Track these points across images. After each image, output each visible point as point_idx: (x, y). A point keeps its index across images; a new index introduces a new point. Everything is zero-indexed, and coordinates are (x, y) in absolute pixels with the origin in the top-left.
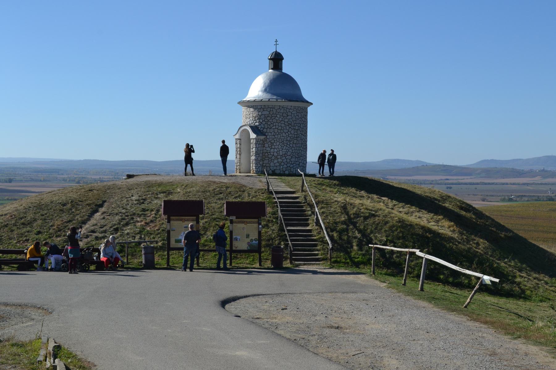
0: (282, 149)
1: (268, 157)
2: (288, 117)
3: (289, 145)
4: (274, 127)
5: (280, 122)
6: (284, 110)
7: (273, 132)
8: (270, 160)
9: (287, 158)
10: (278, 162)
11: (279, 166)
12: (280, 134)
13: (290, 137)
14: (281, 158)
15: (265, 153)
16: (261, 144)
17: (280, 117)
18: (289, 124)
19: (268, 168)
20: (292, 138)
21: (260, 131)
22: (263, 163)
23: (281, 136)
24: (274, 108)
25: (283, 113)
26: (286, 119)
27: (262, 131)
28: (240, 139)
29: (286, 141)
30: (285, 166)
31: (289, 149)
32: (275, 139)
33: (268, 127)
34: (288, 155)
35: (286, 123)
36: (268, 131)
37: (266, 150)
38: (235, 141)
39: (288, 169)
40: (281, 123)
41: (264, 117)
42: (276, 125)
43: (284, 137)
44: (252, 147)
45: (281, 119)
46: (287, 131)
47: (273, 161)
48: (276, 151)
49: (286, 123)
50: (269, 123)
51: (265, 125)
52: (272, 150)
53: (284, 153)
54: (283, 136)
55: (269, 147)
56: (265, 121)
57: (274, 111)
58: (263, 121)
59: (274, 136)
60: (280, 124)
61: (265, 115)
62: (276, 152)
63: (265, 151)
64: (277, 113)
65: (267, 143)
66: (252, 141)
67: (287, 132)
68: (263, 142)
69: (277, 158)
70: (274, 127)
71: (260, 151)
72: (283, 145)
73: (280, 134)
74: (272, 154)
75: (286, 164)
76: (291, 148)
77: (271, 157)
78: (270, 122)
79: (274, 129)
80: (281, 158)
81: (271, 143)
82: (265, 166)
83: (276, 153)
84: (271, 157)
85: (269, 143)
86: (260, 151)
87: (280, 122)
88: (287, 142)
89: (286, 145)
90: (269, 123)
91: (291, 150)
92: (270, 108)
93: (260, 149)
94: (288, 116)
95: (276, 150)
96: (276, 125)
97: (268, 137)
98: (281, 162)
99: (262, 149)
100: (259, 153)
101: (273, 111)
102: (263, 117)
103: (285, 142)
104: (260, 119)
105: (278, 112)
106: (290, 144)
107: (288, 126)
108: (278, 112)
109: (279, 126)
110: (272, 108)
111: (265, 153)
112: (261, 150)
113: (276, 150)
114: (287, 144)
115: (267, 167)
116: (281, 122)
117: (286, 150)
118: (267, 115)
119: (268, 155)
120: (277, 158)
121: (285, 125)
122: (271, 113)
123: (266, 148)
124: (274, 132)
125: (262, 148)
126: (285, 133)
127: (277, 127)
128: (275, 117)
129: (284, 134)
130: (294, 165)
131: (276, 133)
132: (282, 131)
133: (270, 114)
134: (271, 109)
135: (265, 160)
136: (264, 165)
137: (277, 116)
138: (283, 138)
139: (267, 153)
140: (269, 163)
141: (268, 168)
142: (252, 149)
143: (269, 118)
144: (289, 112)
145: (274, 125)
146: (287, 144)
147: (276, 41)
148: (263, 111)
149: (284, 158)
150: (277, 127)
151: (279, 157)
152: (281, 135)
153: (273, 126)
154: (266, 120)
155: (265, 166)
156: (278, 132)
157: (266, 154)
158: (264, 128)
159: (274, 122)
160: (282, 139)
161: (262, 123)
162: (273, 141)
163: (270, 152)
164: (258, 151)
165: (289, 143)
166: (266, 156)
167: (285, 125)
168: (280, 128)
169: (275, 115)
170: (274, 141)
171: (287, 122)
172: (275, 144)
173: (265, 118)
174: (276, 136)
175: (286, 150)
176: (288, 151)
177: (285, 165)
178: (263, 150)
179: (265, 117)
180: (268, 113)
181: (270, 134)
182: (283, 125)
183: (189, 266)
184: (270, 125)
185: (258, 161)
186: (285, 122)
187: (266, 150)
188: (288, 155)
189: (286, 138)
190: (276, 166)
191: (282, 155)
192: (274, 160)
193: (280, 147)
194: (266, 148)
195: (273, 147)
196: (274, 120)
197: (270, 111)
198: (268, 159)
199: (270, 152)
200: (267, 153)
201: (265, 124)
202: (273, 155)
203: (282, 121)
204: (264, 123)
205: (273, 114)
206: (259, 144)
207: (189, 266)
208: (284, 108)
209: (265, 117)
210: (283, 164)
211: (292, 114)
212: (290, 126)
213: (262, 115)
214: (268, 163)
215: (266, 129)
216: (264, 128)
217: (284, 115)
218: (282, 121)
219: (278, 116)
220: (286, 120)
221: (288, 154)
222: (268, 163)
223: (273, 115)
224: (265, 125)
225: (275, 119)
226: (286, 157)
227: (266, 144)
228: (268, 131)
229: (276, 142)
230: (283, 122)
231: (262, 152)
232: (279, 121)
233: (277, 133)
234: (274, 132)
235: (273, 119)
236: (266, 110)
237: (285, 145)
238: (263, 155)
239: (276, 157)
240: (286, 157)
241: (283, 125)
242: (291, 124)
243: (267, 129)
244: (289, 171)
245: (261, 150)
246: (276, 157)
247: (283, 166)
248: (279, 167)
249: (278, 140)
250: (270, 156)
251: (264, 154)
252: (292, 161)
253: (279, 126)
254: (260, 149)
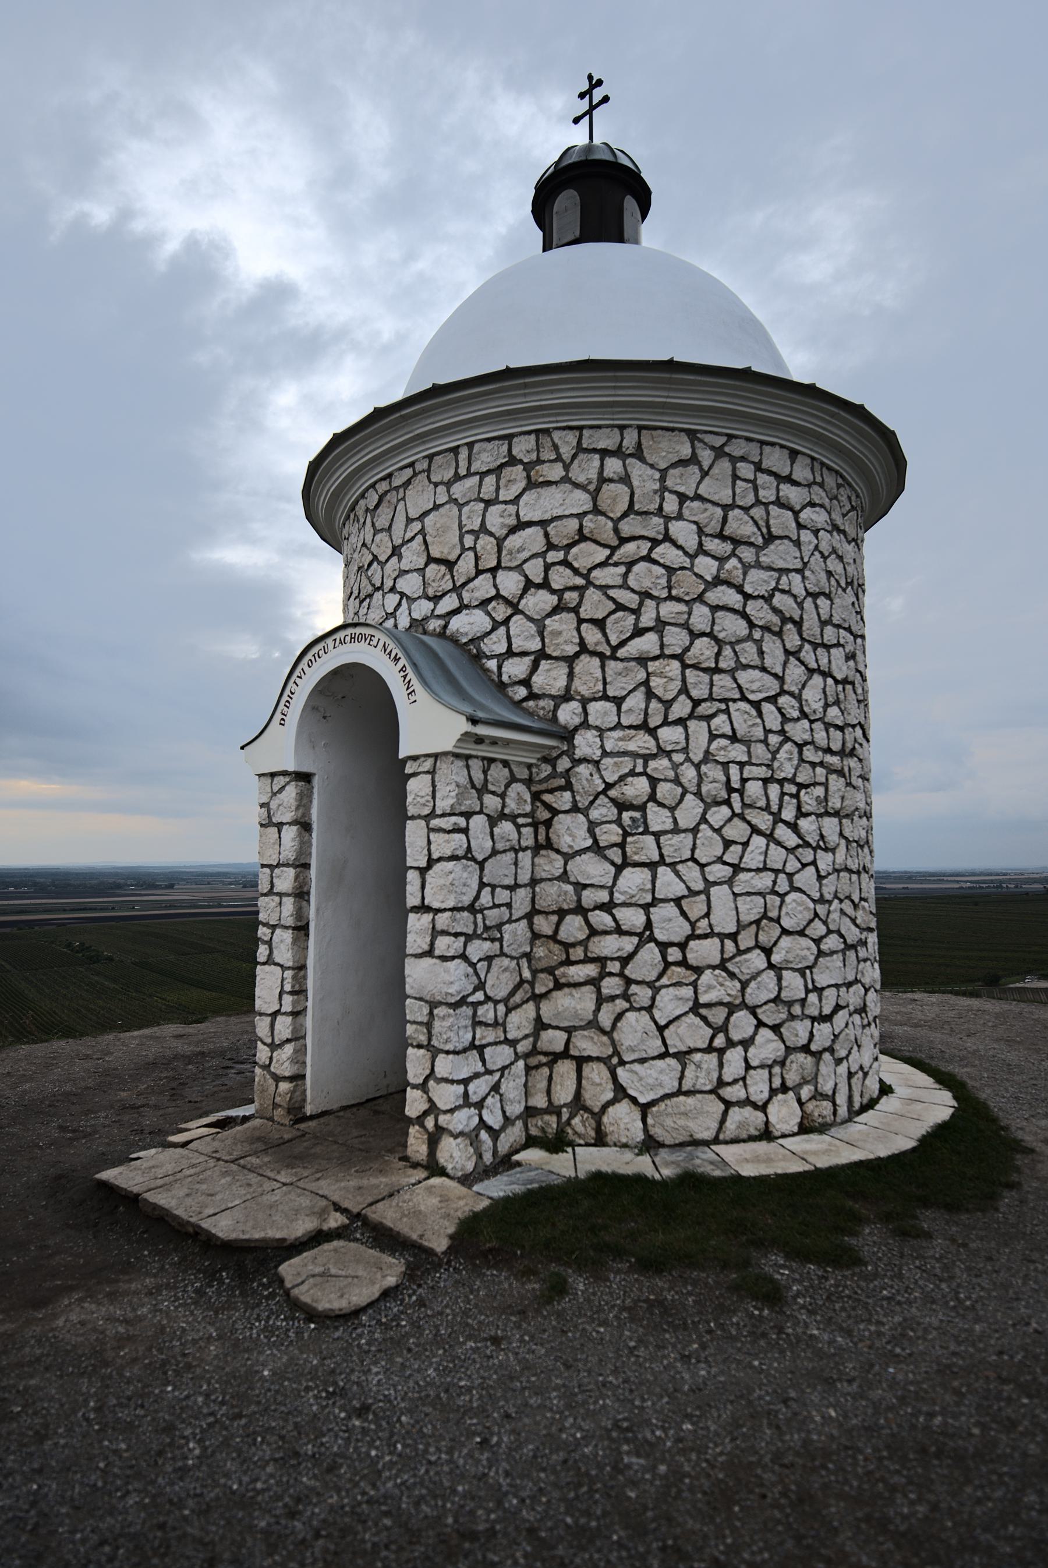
0: (737, 868)
1: (587, 960)
2: (779, 554)
3: (794, 827)
4: (648, 643)
5: (700, 598)
6: (735, 477)
7: (639, 696)
8: (611, 986)
9: (776, 958)
10: (696, 1008)
11: (709, 1049)
12: (704, 709)
13: (800, 747)
14: (722, 966)
15: (562, 913)
16: (513, 818)
17: (701, 550)
18: (785, 620)
19: (596, 1073)
20: (809, 754)
21: (502, 686)
22: (540, 1025)
23: (713, 737)
24: (639, 454)
25: (726, 508)
26: (758, 565)
27: (526, 683)
28: (304, 777)
29: (766, 781)
30: (767, 1048)
31: (792, 865)
32: (660, 766)
33: (583, 648)
34: (785, 932)
35: (758, 611)
36: (581, 687)
37: (564, 877)
38: (255, 792)
39: (792, 1078)
40: (715, 608)
41: (539, 545)
42: (660, 626)
43: (747, 743)
44: (415, 857)
45: (707, 566)
46: (774, 687)
47: (642, 995)
48: (680, 890)
49: (758, 611)
50: (594, 605)
51: (552, 624)
52: (633, 880)
53: (751, 909)
54: (734, 738)
55: (597, 848)
56: (545, 585)
57: (644, 478)
58: (529, 585)
59: (652, 732)
60: (700, 617)
61: (543, 523)
62: (678, 901)
63: (552, 894)
64: (671, 505)
65: (575, 809)
66: (417, 788)
67: (772, 699)
68: (536, 796)
69: (684, 963)
70: (648, 643)
71: (503, 896)
72: (737, 831)
73: (704, 709)
74: (632, 918)
75: (776, 1029)
76: (807, 855)
77: (626, 961)
78: (604, 588)
79: (642, 661)
80: (722, 966)
81: (622, 806)
82: (555, 1057)
83: (671, 910)
84: (626, 961)
85: (602, 811)
86: (503, 896)
87: (700, 598)
88: (774, 790)
89: (763, 821)
90: (594, 605)
91: (806, 878)
92: (604, 453)
93: (500, 870)
94: (770, 538)
95: (668, 883)
96: (660, 626)
97: (586, 743)
98: (732, 1008)
99: (524, 877)
100: (493, 916)
101: (625, 479)
102: (532, 539)
103: (754, 789)
104: (493, 571)
105: (682, 498)
106: (801, 814)
107: (779, 634)
108: (682, 498)
109: (694, 635)
110: (618, 452)
111: (562, 913)
112: (512, 888)
113: (668, 883)
114: (777, 819)
115: (581, 1061)
116: (714, 596)
117: (765, 881)
118: (574, 524)
119: (593, 932)
120: (684, 963)
121: (751, 625)
122: (615, 497)
123: (568, 857)
124: (650, 695)
125: (525, 858)
126: (757, 705)
127: (676, 639)
128: (655, 543)
129: (742, 716)
130: (841, 1018)
131: (668, 704)
132: (723, 684)
133: (596, 511)
134: (613, 466)
135: (558, 986)
136: (552, 1039)
137: (667, 538)
138: (738, 752)
139: (581, 910)
140: (605, 1019)
141: (596, 1073)
142: (423, 871)
143: (587, 555)
144: (779, 503)
145: (647, 619)
146: (777, 819)
147: (595, 83)
148: (531, 484)
149: (757, 960)
150: (676, 639)
151: (705, 951)
152: (720, 723)
153: (639, 632)
154: (560, 578)
155: (565, 1054)
156: (684, 690)
157: (573, 928)
158: (541, 655)
159: (646, 595)
160: (725, 765)
161: (517, 611)
162: (638, 788)
163: (608, 907)
164: (485, 899)
165: (788, 814)
166: (567, 946)
167: (751, 625)
168: (703, 650)
169: (654, 526)
170: (654, 782)
171: (768, 599)
172: (659, 820)
173: (553, 556)
174: (670, 735)
175: (765, 881)
176: (783, 885)
177: (765, 1033)
178: (534, 882)
179: (551, 546)
180: (580, 501)
181: (601, 712)
182: (731, 626)
183: (482, 730)
184: (600, 624)
185: (486, 1012)
186: (747, 597)
187: (564, 877)
188: (785, 932)
189: (760, 752)
190: (681, 1057)
191: (734, 937)
192: (654, 987)
193: (709, 847)
194: (568, 857)
195: (645, 848)
196: (644, 576)
197: (602, 480)
198: (594, 982)
199: (608, 907)
200: (581, 910)
201: (556, 610)
202: (646, 935)
203: (718, 581)
204: (539, 602)
205: (630, 510)
206: (493, 822)
207: (482, 730)
208: (734, 460)
209: (551, 546)
210: (742, 1024)
211: (800, 526)
212: (792, 640)
213: (521, 525)
214: (593, 1024)
215: (562, 670)
216: (541, 655)
217: (740, 525)
218: (718, 581)
219: (683, 532)
220: (757, 582)
221: (786, 923)
222: (593, 1024)
223: (627, 528)
224: (552, 624)
225: (648, 558)
226: (768, 952)
227: (562, 822)
228: (578, 685)
229: (665, 790)
230: (733, 598)
231: (521, 900)
232: (687, 585)
233: (681, 708)
234: (650, 695)
235: (630, 565)
236: (556, 472)
237: (755, 830)
238: (536, 936)
239: (674, 954)
240: (768, 952)
241: (731, 626)
242: (798, 624)
243: (570, 661)
244: (806, 1092)
245: (512, 888)
246: (674, 954)
247: (747, 1043)
248: (713, 1058)
249: (689, 774)
250: (609, 946)
251: (545, 926)
252: (820, 991)
253: (694, 635)
254: (500, 870)
